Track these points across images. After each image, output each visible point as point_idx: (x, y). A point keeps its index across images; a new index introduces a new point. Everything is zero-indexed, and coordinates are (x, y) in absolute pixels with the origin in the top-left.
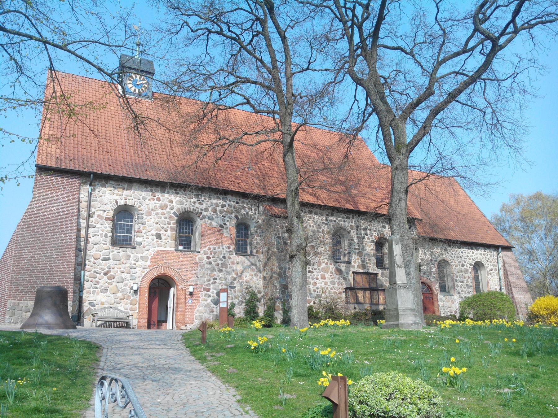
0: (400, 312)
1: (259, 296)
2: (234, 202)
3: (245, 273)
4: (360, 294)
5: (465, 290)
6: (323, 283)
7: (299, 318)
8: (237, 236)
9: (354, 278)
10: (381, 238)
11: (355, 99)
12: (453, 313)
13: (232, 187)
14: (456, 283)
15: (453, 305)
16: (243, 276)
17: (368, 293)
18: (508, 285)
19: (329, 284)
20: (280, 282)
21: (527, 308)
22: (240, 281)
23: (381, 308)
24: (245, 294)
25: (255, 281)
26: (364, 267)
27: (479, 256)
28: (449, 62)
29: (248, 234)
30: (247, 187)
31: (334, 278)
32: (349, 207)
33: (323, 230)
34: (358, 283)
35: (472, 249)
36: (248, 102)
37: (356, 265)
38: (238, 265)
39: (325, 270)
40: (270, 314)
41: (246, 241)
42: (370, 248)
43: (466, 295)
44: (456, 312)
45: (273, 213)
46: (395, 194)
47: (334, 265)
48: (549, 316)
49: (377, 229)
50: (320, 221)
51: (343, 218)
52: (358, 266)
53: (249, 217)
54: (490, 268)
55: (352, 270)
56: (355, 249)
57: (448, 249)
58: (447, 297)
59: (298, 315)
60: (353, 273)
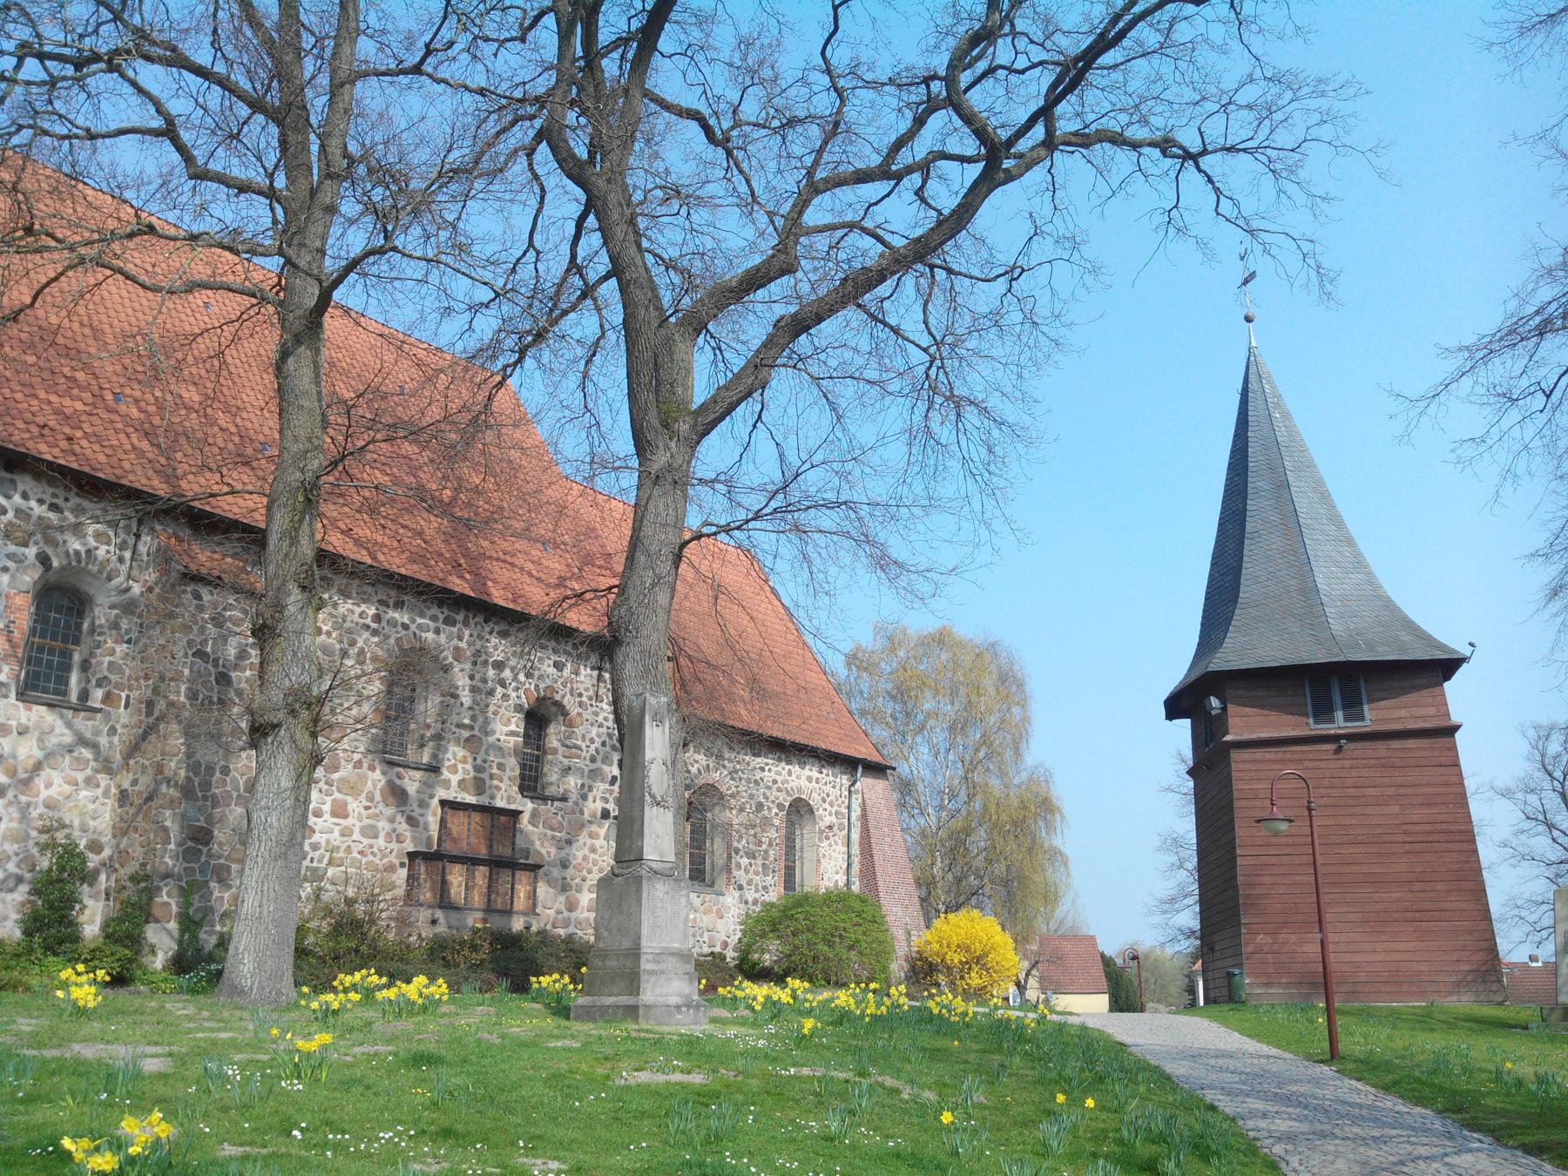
0: (646, 965)
1: (93, 861)
2: (41, 501)
3: (46, 773)
4: (456, 878)
5: (757, 879)
6: (337, 830)
7: (260, 965)
8: (33, 631)
9: (443, 822)
10: (544, 698)
11: (531, 244)
12: (718, 949)
13: (43, 448)
14: (736, 859)
15: (720, 924)
16: (39, 782)
17: (481, 872)
18: (869, 873)
19: (356, 836)
20: (183, 817)
21: (909, 941)
22: (23, 799)
23: (517, 925)
24: (35, 851)
25: (85, 804)
26: (479, 786)
27: (804, 783)
28: (846, 194)
29: (79, 627)
30: (102, 458)
31: (376, 816)
32: (460, 585)
33: (362, 652)
34: (454, 840)
35: (789, 762)
36: (169, 131)
37: (455, 781)
38: (22, 740)
39: (352, 789)
40: (125, 933)
41: (67, 655)
42: (506, 729)
43: (757, 895)
44: (725, 945)
45: (193, 567)
46: (641, 559)
47: (384, 773)
48: (966, 967)
49: (521, 674)
50: (356, 617)
51: (434, 618)
52: (461, 782)
53: (94, 568)
54: (828, 820)
55: (442, 794)
56: (460, 726)
57: (727, 755)
58: (708, 897)
59: (255, 954)
60: (443, 803)
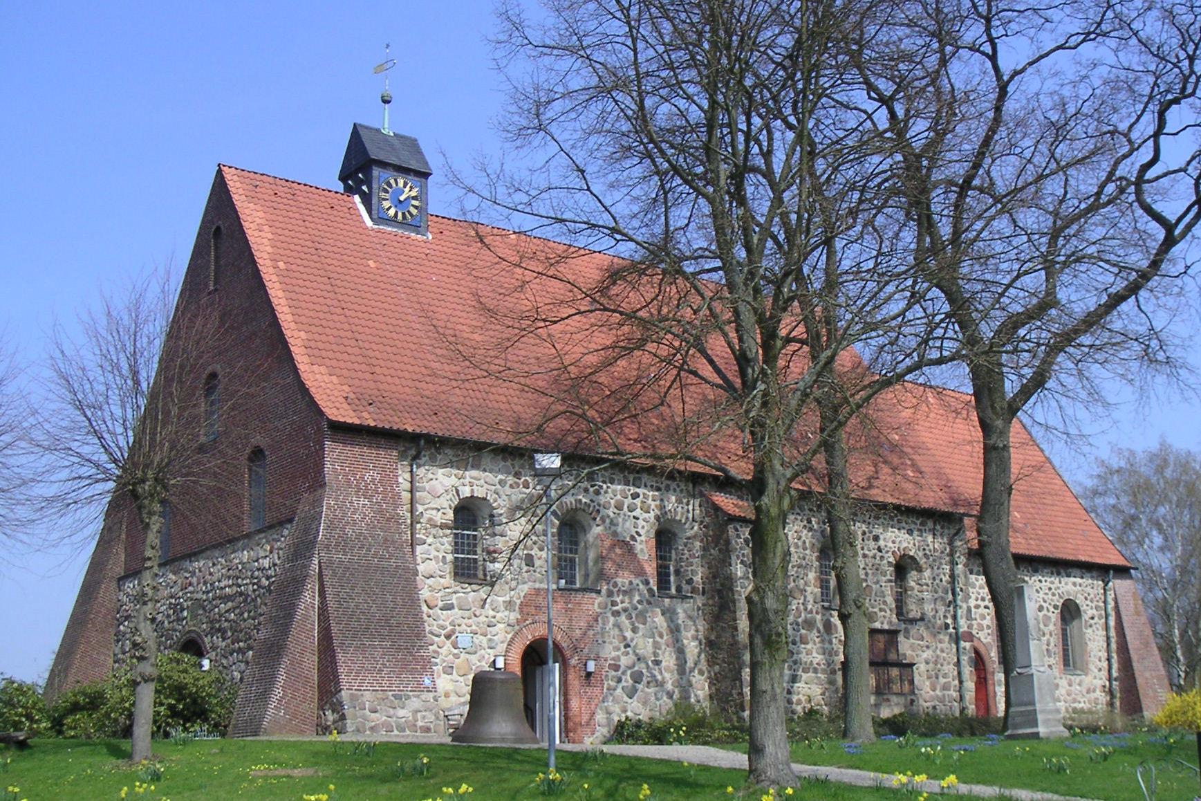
27: (1070, 587)
